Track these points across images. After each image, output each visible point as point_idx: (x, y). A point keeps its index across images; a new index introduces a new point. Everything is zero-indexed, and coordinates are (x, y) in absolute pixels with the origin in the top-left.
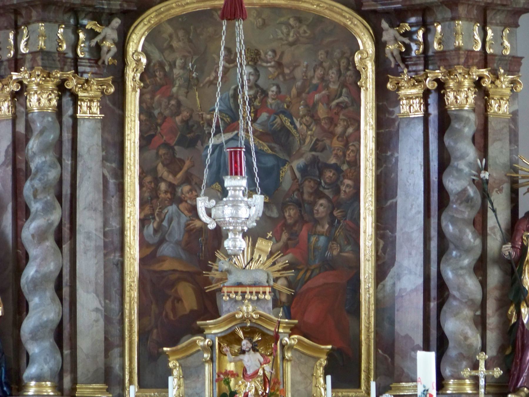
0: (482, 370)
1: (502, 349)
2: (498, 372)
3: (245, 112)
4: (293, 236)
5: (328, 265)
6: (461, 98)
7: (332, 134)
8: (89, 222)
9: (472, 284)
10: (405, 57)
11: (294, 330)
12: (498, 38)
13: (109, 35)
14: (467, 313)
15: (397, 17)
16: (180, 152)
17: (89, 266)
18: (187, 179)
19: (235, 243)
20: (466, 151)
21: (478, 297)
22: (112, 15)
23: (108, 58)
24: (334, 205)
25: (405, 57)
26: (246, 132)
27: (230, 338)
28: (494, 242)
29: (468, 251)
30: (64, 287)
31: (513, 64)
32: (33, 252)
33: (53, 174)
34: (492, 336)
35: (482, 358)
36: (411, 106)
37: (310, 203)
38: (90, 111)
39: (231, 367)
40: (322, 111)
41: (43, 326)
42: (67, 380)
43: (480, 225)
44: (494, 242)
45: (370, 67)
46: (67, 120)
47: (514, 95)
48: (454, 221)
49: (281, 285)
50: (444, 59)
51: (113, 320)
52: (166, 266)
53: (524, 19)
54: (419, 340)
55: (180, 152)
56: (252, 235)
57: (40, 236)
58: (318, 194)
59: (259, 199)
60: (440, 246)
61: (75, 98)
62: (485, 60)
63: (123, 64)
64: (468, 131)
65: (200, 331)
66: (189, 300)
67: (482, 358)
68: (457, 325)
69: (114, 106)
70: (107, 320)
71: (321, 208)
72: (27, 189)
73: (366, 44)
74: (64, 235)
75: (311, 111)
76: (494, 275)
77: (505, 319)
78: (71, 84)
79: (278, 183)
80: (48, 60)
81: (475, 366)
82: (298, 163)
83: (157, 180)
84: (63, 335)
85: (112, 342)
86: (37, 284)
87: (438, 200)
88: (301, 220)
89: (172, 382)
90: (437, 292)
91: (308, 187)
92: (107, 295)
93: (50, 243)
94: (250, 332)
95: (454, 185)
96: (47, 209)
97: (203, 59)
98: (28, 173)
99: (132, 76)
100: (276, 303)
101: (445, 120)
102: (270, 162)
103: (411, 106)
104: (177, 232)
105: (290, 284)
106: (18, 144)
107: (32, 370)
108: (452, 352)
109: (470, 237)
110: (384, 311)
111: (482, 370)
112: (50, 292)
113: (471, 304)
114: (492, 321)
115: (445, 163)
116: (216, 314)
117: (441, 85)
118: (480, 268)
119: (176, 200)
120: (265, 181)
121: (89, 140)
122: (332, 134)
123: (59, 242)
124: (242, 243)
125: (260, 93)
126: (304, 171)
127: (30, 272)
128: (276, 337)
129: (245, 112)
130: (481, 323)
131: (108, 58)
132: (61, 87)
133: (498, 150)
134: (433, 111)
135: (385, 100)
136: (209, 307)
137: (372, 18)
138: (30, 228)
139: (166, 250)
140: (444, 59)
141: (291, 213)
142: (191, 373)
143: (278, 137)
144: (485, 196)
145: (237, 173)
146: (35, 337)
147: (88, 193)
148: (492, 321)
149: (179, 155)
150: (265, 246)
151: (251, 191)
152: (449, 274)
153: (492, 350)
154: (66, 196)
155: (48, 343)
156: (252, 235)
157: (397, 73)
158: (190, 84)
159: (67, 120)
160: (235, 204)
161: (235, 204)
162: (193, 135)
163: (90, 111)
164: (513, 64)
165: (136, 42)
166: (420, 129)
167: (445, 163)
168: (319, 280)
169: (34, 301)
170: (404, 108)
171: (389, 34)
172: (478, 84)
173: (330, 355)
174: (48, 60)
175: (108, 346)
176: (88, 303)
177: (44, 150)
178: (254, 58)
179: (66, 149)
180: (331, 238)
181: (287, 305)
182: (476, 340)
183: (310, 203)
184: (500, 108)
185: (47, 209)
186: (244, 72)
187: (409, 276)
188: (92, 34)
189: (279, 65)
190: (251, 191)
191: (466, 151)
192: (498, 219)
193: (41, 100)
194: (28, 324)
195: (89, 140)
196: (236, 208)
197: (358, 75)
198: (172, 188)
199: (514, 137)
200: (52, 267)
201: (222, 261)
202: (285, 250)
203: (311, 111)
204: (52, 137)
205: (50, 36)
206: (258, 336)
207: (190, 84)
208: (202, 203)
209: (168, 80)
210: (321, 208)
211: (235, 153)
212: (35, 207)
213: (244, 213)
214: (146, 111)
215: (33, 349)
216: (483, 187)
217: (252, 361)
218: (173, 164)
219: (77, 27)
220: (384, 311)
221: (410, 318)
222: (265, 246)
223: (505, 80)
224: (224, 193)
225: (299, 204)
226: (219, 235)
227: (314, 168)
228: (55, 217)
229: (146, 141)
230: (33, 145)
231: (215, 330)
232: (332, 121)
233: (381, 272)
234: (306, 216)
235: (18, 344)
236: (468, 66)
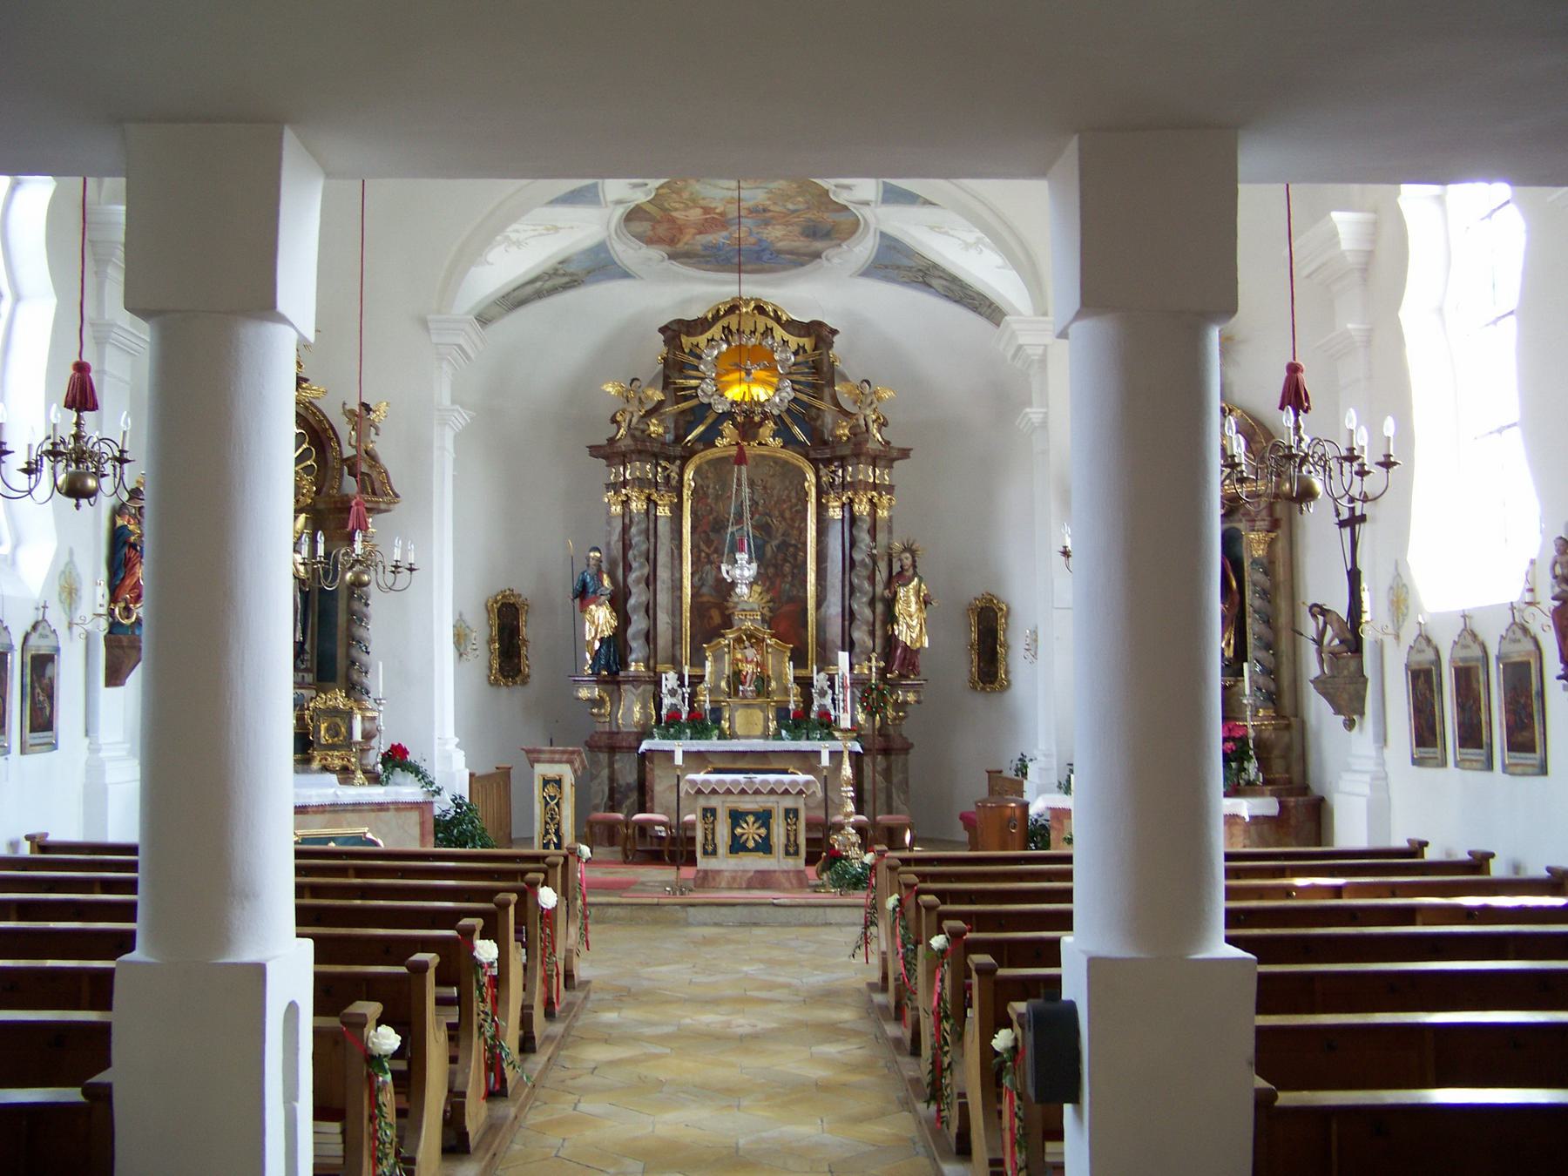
0: (874, 663)
1: (884, 649)
2: (882, 664)
3: (747, 515)
4: (772, 583)
5: (791, 600)
6: (862, 508)
7: (792, 527)
8: (663, 574)
9: (867, 612)
10: (832, 484)
11: (773, 636)
12: (882, 474)
13: (674, 470)
14: (865, 628)
15: (828, 462)
16: (712, 536)
17: (663, 598)
18: (716, 551)
19: (742, 590)
20: (864, 537)
21: (871, 619)
22: (675, 458)
23: (674, 483)
24: (794, 566)
25: (832, 484)
26: (748, 526)
27: (739, 640)
28: (879, 589)
29: (865, 593)
30: (650, 610)
31: (890, 489)
32: (634, 590)
33: (644, 547)
34: (878, 641)
35: (874, 656)
36: (835, 513)
37: (780, 566)
38: (663, 512)
39: (739, 656)
40: (787, 514)
41: (639, 632)
42: (652, 663)
43: (872, 579)
44: (879, 589)
45: (813, 490)
46: (652, 517)
47: (890, 507)
48: (858, 577)
49: (766, 611)
50: (853, 486)
51: (676, 629)
52: (705, 599)
53: (896, 464)
54: (839, 643)
55: (712, 536)
56: (750, 585)
57: (638, 581)
58: (785, 560)
59: (754, 565)
60: (850, 591)
61: (656, 505)
62: (875, 487)
63: (681, 485)
64: (866, 526)
65: (723, 636)
66: (717, 619)
67: (874, 656)
68: (860, 635)
69: (677, 509)
70: (674, 629)
71: (787, 568)
72: (630, 554)
73: (811, 477)
74: (650, 581)
75: (782, 515)
76: (880, 607)
77: (886, 632)
78: (655, 497)
79: (764, 553)
80: (641, 483)
81: (870, 660)
82: (774, 543)
83: (700, 551)
84: (650, 637)
85: (676, 641)
86: (635, 609)
87: (850, 565)
88: (776, 575)
89: (708, 664)
90: (849, 616)
91: (780, 556)
92: (673, 614)
93: (643, 585)
94: (749, 637)
95: (857, 556)
96: (642, 566)
97: (725, 485)
98: (631, 545)
99: (686, 493)
100: (763, 620)
101: (853, 520)
102: (759, 542)
103: (835, 513)
104: (710, 581)
105: (771, 610)
106: (625, 529)
107: (633, 656)
108: (857, 650)
109: (866, 586)
110: (821, 626)
111: (874, 663)
112: (642, 613)
113: (867, 623)
114: (879, 633)
115: (853, 544)
116: (731, 627)
117: (851, 501)
118: (872, 603)
119: (710, 562)
120: (759, 556)
121: (664, 529)
122: (792, 527)
123: (647, 611)
124: (745, 590)
125: (754, 503)
126: (778, 547)
127: (632, 601)
128: (763, 640)
129: (747, 515)
130: (872, 634)
131: (674, 483)
132: (648, 498)
133: (882, 537)
134: (847, 515)
135: (821, 508)
136: (728, 622)
137: (814, 462)
138: (633, 576)
139: (705, 590)
140: (853, 486)
141: (771, 571)
142: (718, 659)
143: (764, 529)
144: (875, 563)
145: (742, 550)
146: (634, 638)
147: (663, 558)
148: (879, 633)
149: (712, 541)
150: (757, 589)
151: (750, 562)
152: (855, 607)
153: (878, 650)
154: (651, 559)
155: (642, 641)
156: (750, 585)
157: (828, 494)
158: (718, 498)
159: (652, 517)
160: (742, 568)
161: (742, 568)
162: (719, 526)
163: (663, 512)
164: (890, 489)
165: (689, 474)
166: (839, 525)
167: (853, 544)
168: (786, 608)
169: (634, 618)
170: (831, 512)
171: (823, 471)
172: (871, 500)
173: (792, 650)
174: (641, 483)
175: (674, 643)
176: (663, 619)
177: (640, 533)
178: (752, 484)
179: (651, 532)
180: (793, 585)
181: (769, 622)
182: (870, 643)
183: (780, 566)
184: (882, 513)
185: (642, 566)
186: (746, 490)
187: (834, 608)
188: (665, 469)
189: (765, 488)
190: (750, 562)
191: (864, 537)
192: (882, 576)
193: (637, 506)
194: (631, 631)
195: (664, 529)
196: (742, 570)
197: (807, 494)
198: (708, 555)
199: (890, 531)
200: (644, 599)
201: (703, 345)
202: (767, 591)
203: (782, 515)
204: (643, 526)
205: (642, 469)
206: (754, 639)
207: (718, 498)
208: (724, 568)
209: (706, 495)
210: (787, 568)
211: (742, 541)
212: (635, 565)
213: (747, 573)
214: (693, 512)
215: (634, 644)
216: (873, 558)
217: (750, 653)
218: (709, 542)
219: (657, 464)
220: (821, 626)
221: (835, 630)
222: (757, 589)
223: (886, 498)
224: (736, 561)
225: (775, 566)
226: (733, 584)
227: (784, 545)
228: (646, 571)
229: (693, 528)
230: (633, 530)
231: (731, 635)
232: (793, 520)
233: (819, 603)
234: (779, 573)
235: (626, 641)
236: (865, 490)
